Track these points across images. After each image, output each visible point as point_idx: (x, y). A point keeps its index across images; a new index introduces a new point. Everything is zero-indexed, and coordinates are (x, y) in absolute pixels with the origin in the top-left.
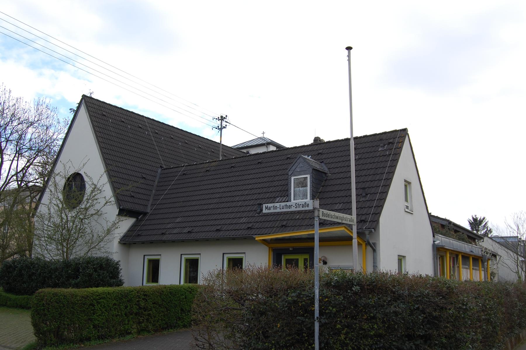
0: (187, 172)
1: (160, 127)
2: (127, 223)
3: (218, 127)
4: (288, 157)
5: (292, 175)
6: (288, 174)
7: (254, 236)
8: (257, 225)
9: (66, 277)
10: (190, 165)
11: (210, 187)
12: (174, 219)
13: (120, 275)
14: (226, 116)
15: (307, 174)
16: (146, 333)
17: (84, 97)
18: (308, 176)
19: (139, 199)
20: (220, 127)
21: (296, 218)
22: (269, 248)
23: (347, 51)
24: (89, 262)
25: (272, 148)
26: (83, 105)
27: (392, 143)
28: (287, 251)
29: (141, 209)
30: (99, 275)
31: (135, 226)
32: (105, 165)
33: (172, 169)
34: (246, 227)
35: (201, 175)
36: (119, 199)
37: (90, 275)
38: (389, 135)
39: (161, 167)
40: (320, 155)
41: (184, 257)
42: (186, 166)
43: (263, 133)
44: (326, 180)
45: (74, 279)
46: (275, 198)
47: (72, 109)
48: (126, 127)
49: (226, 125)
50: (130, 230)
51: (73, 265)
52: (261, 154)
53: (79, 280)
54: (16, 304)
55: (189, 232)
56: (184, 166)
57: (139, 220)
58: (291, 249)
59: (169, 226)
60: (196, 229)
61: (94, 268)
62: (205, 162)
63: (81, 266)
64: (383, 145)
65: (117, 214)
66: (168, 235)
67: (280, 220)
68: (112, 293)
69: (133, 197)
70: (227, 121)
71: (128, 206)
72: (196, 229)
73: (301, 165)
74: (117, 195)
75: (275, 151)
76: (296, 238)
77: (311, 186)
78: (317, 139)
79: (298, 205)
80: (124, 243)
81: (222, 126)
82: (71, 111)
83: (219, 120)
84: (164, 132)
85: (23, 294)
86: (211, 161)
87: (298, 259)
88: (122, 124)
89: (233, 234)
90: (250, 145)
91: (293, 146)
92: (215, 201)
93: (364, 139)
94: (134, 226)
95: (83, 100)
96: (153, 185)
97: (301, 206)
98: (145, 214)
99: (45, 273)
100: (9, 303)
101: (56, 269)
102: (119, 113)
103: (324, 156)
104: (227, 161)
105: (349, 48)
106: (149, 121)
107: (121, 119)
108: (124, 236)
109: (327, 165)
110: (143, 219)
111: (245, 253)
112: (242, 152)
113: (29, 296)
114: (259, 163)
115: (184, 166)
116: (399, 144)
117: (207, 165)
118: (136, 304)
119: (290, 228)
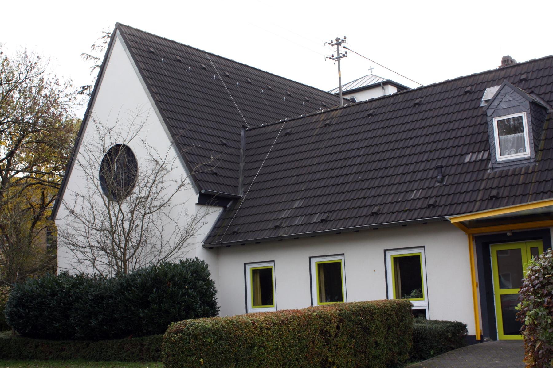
0: (291, 131)
1: (230, 67)
3: (333, 56)
4: (369, 113)
5: (493, 116)
6: (486, 115)
7: (448, 218)
10: (293, 120)
12: (290, 203)
14: (345, 38)
15: (521, 111)
17: (119, 26)
18: (524, 115)
20: (336, 56)
22: (469, 235)
25: (391, 91)
26: (117, 38)
28: (501, 238)
29: (229, 192)
31: (223, 219)
33: (264, 129)
34: (370, 213)
39: (244, 127)
40: (327, 126)
41: (389, 255)
42: (287, 121)
46: (462, 155)
47: (84, 54)
48: (185, 69)
49: (346, 53)
50: (217, 227)
52: (365, 102)
55: (322, 221)
56: (282, 122)
57: (227, 210)
58: (509, 234)
60: (333, 216)
62: (318, 112)
65: (197, 202)
67: (484, 189)
69: (216, 174)
70: (345, 46)
72: (333, 216)
73: (508, 98)
75: (394, 95)
77: (531, 131)
78: (506, 60)
81: (338, 55)
83: (332, 45)
84: (236, 74)
86: (307, 115)
87: (520, 249)
88: (178, 63)
89: (403, 218)
90: (348, 89)
91: (442, 80)
95: (118, 32)
96: (239, 154)
98: (237, 199)
102: (170, 48)
103: (532, 84)
104: (253, 131)
106: (214, 59)
107: (176, 57)
109: (542, 96)
111: (423, 247)
115: (282, 122)
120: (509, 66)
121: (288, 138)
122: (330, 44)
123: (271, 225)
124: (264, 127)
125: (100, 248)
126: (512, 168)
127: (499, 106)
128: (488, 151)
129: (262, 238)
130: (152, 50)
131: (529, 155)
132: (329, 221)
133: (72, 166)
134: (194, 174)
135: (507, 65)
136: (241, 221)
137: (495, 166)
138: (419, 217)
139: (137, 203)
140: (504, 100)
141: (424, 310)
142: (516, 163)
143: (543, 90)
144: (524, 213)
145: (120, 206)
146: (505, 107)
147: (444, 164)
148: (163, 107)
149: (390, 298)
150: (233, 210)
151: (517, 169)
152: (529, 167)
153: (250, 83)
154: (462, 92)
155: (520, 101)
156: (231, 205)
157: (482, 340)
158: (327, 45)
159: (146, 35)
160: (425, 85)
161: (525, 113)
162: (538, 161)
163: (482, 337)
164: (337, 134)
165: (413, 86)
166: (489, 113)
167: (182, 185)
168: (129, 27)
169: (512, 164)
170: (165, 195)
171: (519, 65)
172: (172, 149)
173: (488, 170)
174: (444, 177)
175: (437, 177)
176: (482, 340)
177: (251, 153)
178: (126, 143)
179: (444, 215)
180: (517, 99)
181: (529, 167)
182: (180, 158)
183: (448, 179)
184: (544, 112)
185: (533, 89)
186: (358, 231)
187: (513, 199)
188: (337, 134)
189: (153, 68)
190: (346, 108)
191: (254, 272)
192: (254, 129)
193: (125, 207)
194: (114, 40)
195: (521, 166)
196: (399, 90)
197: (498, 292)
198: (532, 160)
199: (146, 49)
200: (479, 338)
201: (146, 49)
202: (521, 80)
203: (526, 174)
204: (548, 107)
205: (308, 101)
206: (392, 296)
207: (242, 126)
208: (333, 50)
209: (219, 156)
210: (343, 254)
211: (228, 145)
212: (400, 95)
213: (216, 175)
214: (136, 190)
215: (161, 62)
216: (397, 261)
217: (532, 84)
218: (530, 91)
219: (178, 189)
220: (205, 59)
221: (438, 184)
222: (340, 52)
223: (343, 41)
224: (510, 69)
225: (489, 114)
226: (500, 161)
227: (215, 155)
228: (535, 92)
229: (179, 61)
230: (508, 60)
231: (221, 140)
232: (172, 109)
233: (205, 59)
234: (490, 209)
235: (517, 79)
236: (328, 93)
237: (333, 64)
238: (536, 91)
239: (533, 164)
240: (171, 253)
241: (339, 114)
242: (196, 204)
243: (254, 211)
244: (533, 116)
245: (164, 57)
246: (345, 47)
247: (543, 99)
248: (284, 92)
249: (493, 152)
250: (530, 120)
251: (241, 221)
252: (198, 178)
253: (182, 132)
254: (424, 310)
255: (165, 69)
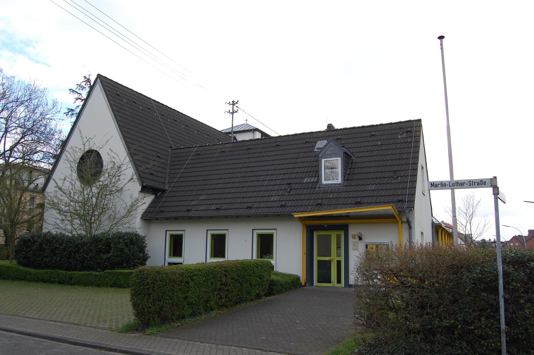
2: (149, 199)
7: (293, 214)
8: (290, 203)
9: (96, 252)
10: (202, 146)
11: (229, 166)
13: (146, 249)
14: (238, 101)
16: (224, 309)
17: (99, 76)
19: (157, 176)
20: (231, 111)
21: (330, 197)
22: (303, 224)
23: (439, 40)
24: (120, 236)
25: (258, 136)
26: (98, 84)
27: (411, 132)
30: (130, 250)
31: (155, 202)
32: (125, 144)
35: (216, 155)
36: (141, 176)
37: (122, 250)
38: (405, 124)
39: (171, 147)
41: (255, 232)
43: (247, 120)
44: (352, 163)
45: (104, 253)
47: (71, 89)
49: (238, 110)
51: (103, 240)
52: (247, 141)
53: (110, 254)
54: (38, 278)
55: (217, 209)
56: (195, 147)
57: (158, 197)
58: (326, 226)
59: (193, 203)
60: (224, 207)
61: (125, 243)
63: (112, 241)
64: (402, 133)
65: (140, 191)
66: (194, 212)
68: (202, 270)
69: (153, 174)
71: (151, 184)
72: (224, 207)
73: (332, 148)
74: (140, 172)
76: (335, 215)
78: (330, 126)
79: (472, 182)
80: (145, 218)
82: (71, 92)
85: (43, 268)
92: (238, 180)
93: (380, 127)
94: (153, 203)
95: (98, 80)
97: (476, 184)
98: (163, 191)
99: (71, 247)
100: (28, 277)
101: (84, 244)
103: (344, 142)
105: (441, 38)
108: (145, 212)
109: (349, 149)
110: (163, 196)
111: (276, 229)
112: (229, 136)
113: (52, 271)
114: (277, 146)
115: (195, 147)
116: (417, 133)
117: (220, 146)
118: (219, 281)
119: (326, 207)
120: (331, 130)
121: (198, 157)
122: (228, 104)
123: (185, 208)
124: (183, 148)
125: (76, 214)
126: (330, 189)
127: (326, 152)
128: (317, 177)
129: (179, 216)
130: (119, 93)
131: (340, 182)
132: (221, 209)
133: (59, 160)
134: (139, 173)
135: (330, 129)
136: (166, 204)
137: (321, 186)
138: (272, 212)
139: (102, 188)
140: (329, 149)
141: (318, 256)
142: (332, 186)
143: (349, 146)
144: (365, 214)
145: (91, 188)
146: (329, 154)
147: (291, 182)
148: (123, 129)
149: (253, 259)
150: (161, 197)
151: (333, 190)
152: (340, 188)
153: (176, 121)
154: (304, 142)
155: (338, 151)
156: (160, 194)
157: (305, 285)
158: (227, 104)
159: (114, 83)
160: (282, 135)
161: (340, 158)
162: (345, 186)
163: (305, 283)
164: (228, 158)
165: (273, 134)
166: (320, 156)
167: (132, 179)
168: (105, 77)
169: (331, 186)
170: (120, 185)
171: (337, 130)
172: (127, 157)
173: (317, 188)
174: (291, 190)
175: (287, 189)
176: (305, 285)
177: (175, 163)
178: (97, 150)
179: (290, 212)
180: (336, 150)
181: (340, 188)
182: (131, 162)
183: (293, 191)
184: (350, 158)
185: (344, 145)
186: (267, 216)
187: (331, 206)
188: (228, 158)
189: (118, 105)
190: (235, 142)
191: (171, 236)
192: (177, 149)
193: (95, 190)
194: (96, 84)
195: (335, 188)
196: (495, 196)
197: (316, 258)
198: (342, 185)
199: (115, 92)
200: (303, 284)
201: (115, 92)
202: (338, 139)
203: (338, 193)
204: (352, 156)
205: (209, 135)
206: (255, 257)
207: (169, 146)
208: (230, 108)
209: (155, 163)
210: (228, 230)
211: (161, 157)
212: (267, 139)
213: (153, 175)
214: (102, 179)
215: (124, 102)
216: (260, 236)
217: (344, 142)
218: (343, 145)
219: (129, 181)
220: (150, 103)
221: (287, 194)
222: (234, 109)
223: (236, 103)
224: (332, 132)
225: (320, 156)
226: (324, 184)
227: (153, 162)
228: (345, 146)
229: (135, 102)
230: (331, 126)
231: (157, 154)
232: (129, 131)
233: (150, 103)
234: (325, 210)
235: (336, 138)
236: (220, 132)
237: (229, 116)
238: (346, 146)
239: (342, 187)
240: (121, 219)
241: (231, 146)
242: (139, 192)
243: (174, 199)
244: (344, 160)
245: (126, 99)
246: (237, 107)
247: (349, 151)
248: (195, 128)
249: (320, 178)
250: (343, 162)
251: (166, 204)
252: (142, 176)
253: (135, 147)
254: (318, 256)
255: (126, 106)
